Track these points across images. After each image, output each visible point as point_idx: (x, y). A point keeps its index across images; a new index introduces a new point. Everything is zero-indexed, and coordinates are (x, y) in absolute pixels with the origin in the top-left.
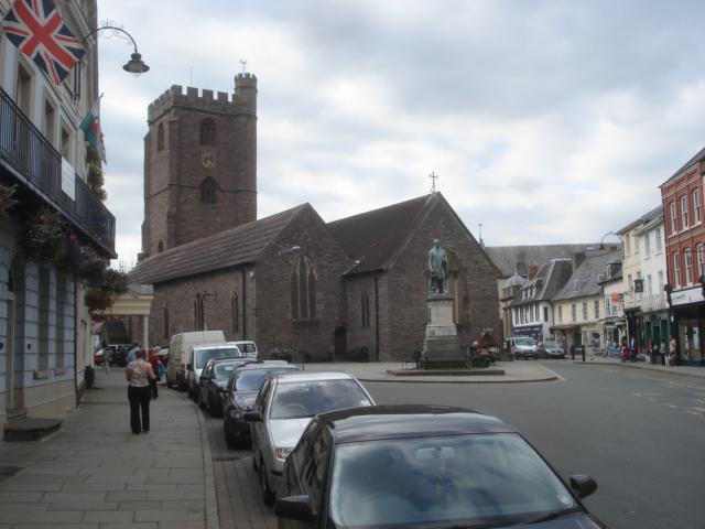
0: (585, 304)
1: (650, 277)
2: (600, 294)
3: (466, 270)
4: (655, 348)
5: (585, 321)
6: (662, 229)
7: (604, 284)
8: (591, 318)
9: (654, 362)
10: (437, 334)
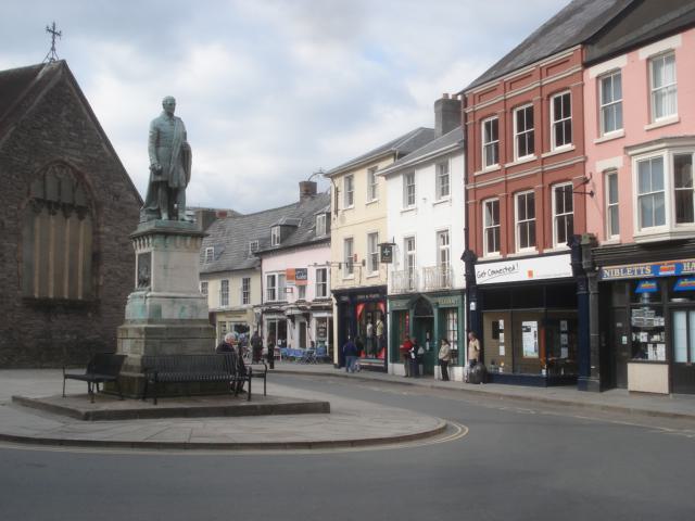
0: (225, 284)
1: (410, 242)
2: (255, 269)
3: (99, 206)
4: (421, 351)
5: (224, 307)
6: (457, 166)
7: (264, 253)
8: (235, 301)
9: (414, 371)
10: (166, 314)
